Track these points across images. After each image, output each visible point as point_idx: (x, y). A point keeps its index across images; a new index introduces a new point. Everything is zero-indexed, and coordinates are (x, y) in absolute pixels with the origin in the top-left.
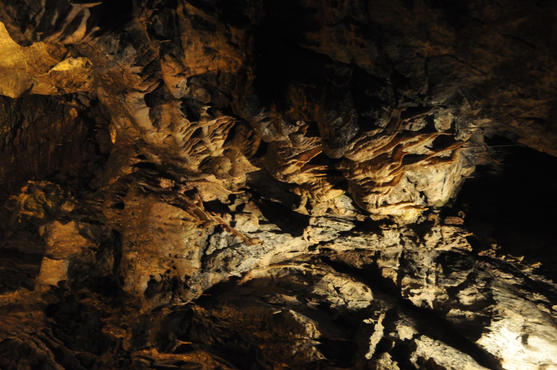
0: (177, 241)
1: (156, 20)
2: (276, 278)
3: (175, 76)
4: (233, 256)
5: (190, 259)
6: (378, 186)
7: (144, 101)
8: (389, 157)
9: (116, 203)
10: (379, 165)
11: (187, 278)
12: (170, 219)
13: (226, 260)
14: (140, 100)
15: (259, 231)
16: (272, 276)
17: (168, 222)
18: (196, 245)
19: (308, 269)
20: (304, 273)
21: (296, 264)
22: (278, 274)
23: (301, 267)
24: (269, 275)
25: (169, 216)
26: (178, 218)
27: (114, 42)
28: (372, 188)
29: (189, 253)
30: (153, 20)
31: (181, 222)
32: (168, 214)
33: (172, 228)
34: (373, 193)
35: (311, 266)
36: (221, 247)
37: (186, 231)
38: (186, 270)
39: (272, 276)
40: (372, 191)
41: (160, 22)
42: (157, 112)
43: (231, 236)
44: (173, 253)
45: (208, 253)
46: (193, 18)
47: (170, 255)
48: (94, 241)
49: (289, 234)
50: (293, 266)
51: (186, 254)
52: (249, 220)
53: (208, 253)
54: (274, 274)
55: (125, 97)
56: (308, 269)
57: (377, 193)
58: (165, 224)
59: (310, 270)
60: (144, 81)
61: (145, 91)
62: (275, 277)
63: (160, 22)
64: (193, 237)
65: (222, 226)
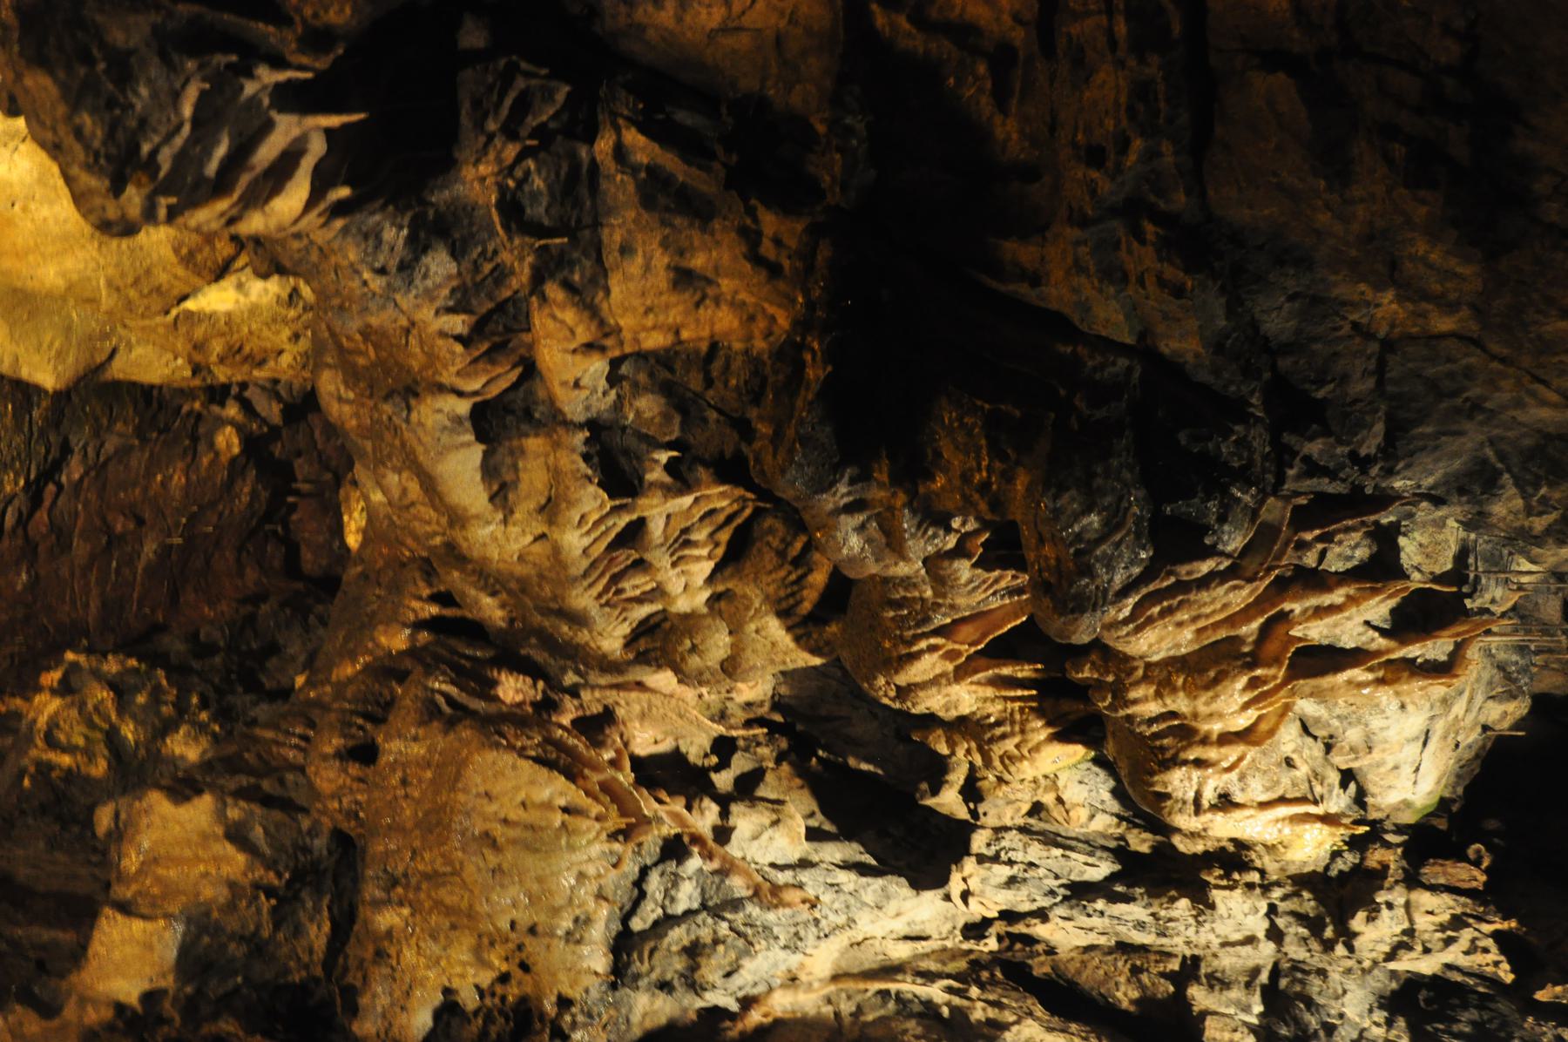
0: (540, 880)
1: (527, 173)
2: (854, 1024)
3: (574, 351)
4: (716, 941)
5: (579, 942)
6: (1205, 741)
7: (468, 424)
8: (1246, 649)
9: (351, 743)
10: (1212, 674)
11: (564, 1003)
12: (523, 804)
13: (694, 951)
14: (457, 420)
15: (804, 864)
16: (837, 1014)
17: (515, 814)
18: (600, 896)
19: (957, 1001)
20: (945, 1011)
21: (919, 980)
22: (859, 1010)
23: (936, 992)
24: (828, 1010)
25: (521, 796)
26: (547, 806)
27: (389, 234)
28: (1184, 749)
29: (576, 920)
30: (519, 173)
31: (558, 819)
32: (517, 789)
33: (528, 835)
34: (1185, 763)
35: (967, 990)
36: (679, 908)
37: (571, 848)
38: (562, 977)
39: (837, 1014)
40: (1183, 756)
41: (538, 183)
42: (508, 460)
43: (714, 873)
44: (524, 918)
45: (637, 924)
46: (643, 175)
47: (513, 924)
48: (271, 865)
49: (903, 880)
50: (908, 986)
51: (566, 923)
52: (775, 823)
53: (637, 924)
54: (847, 1008)
55: (409, 409)
56: (957, 1001)
57: (1200, 763)
58: (505, 821)
59: (965, 1003)
60: (475, 361)
61: (476, 393)
62: (847, 1020)
63: (538, 183)
64: (591, 870)
65: (686, 839)
